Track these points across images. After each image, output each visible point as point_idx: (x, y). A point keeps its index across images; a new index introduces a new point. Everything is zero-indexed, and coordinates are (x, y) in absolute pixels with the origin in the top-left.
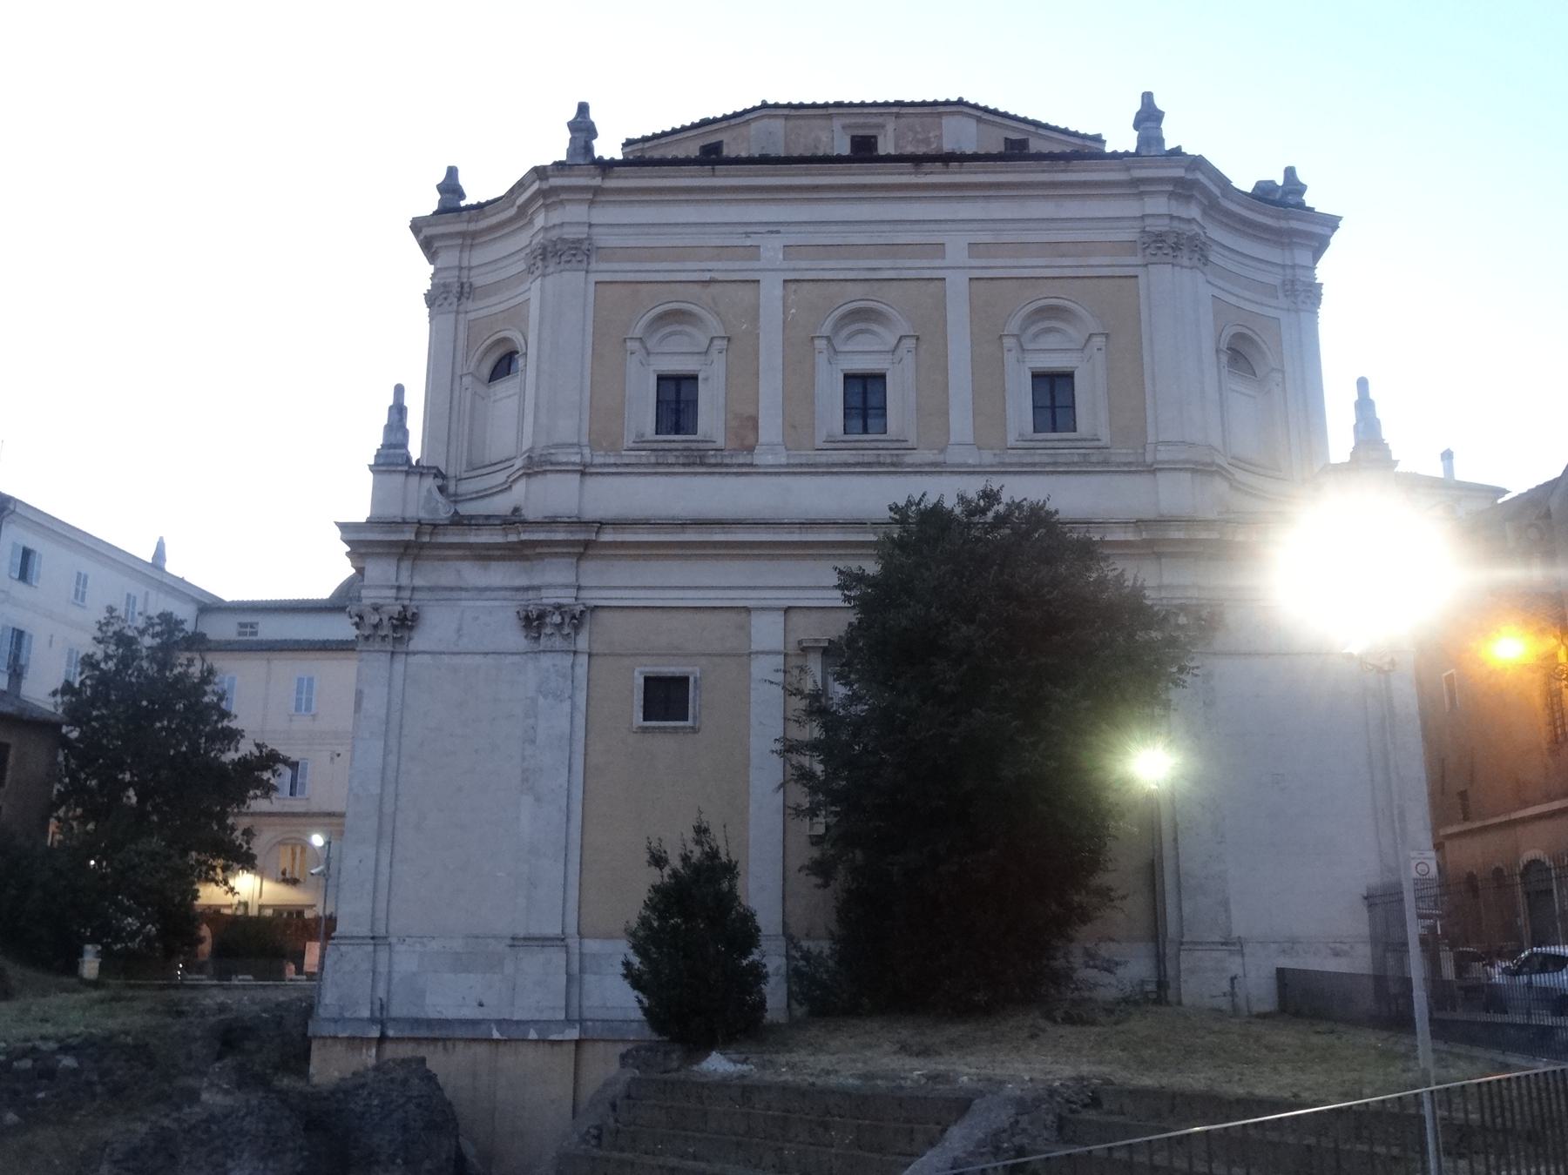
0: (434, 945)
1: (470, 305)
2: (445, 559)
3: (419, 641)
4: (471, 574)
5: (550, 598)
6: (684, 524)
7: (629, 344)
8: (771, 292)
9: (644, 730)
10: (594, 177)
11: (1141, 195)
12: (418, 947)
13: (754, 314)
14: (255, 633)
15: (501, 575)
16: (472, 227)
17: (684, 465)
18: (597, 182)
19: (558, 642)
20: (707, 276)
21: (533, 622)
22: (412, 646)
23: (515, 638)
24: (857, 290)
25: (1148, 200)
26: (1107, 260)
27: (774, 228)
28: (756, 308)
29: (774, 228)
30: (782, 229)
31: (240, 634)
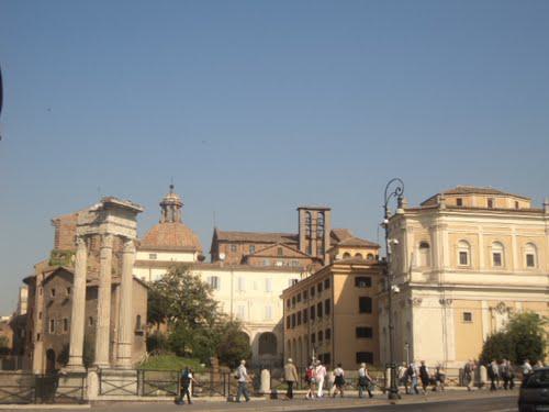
5: (446, 298)
15: (435, 292)
21: (442, 302)
23: (440, 305)
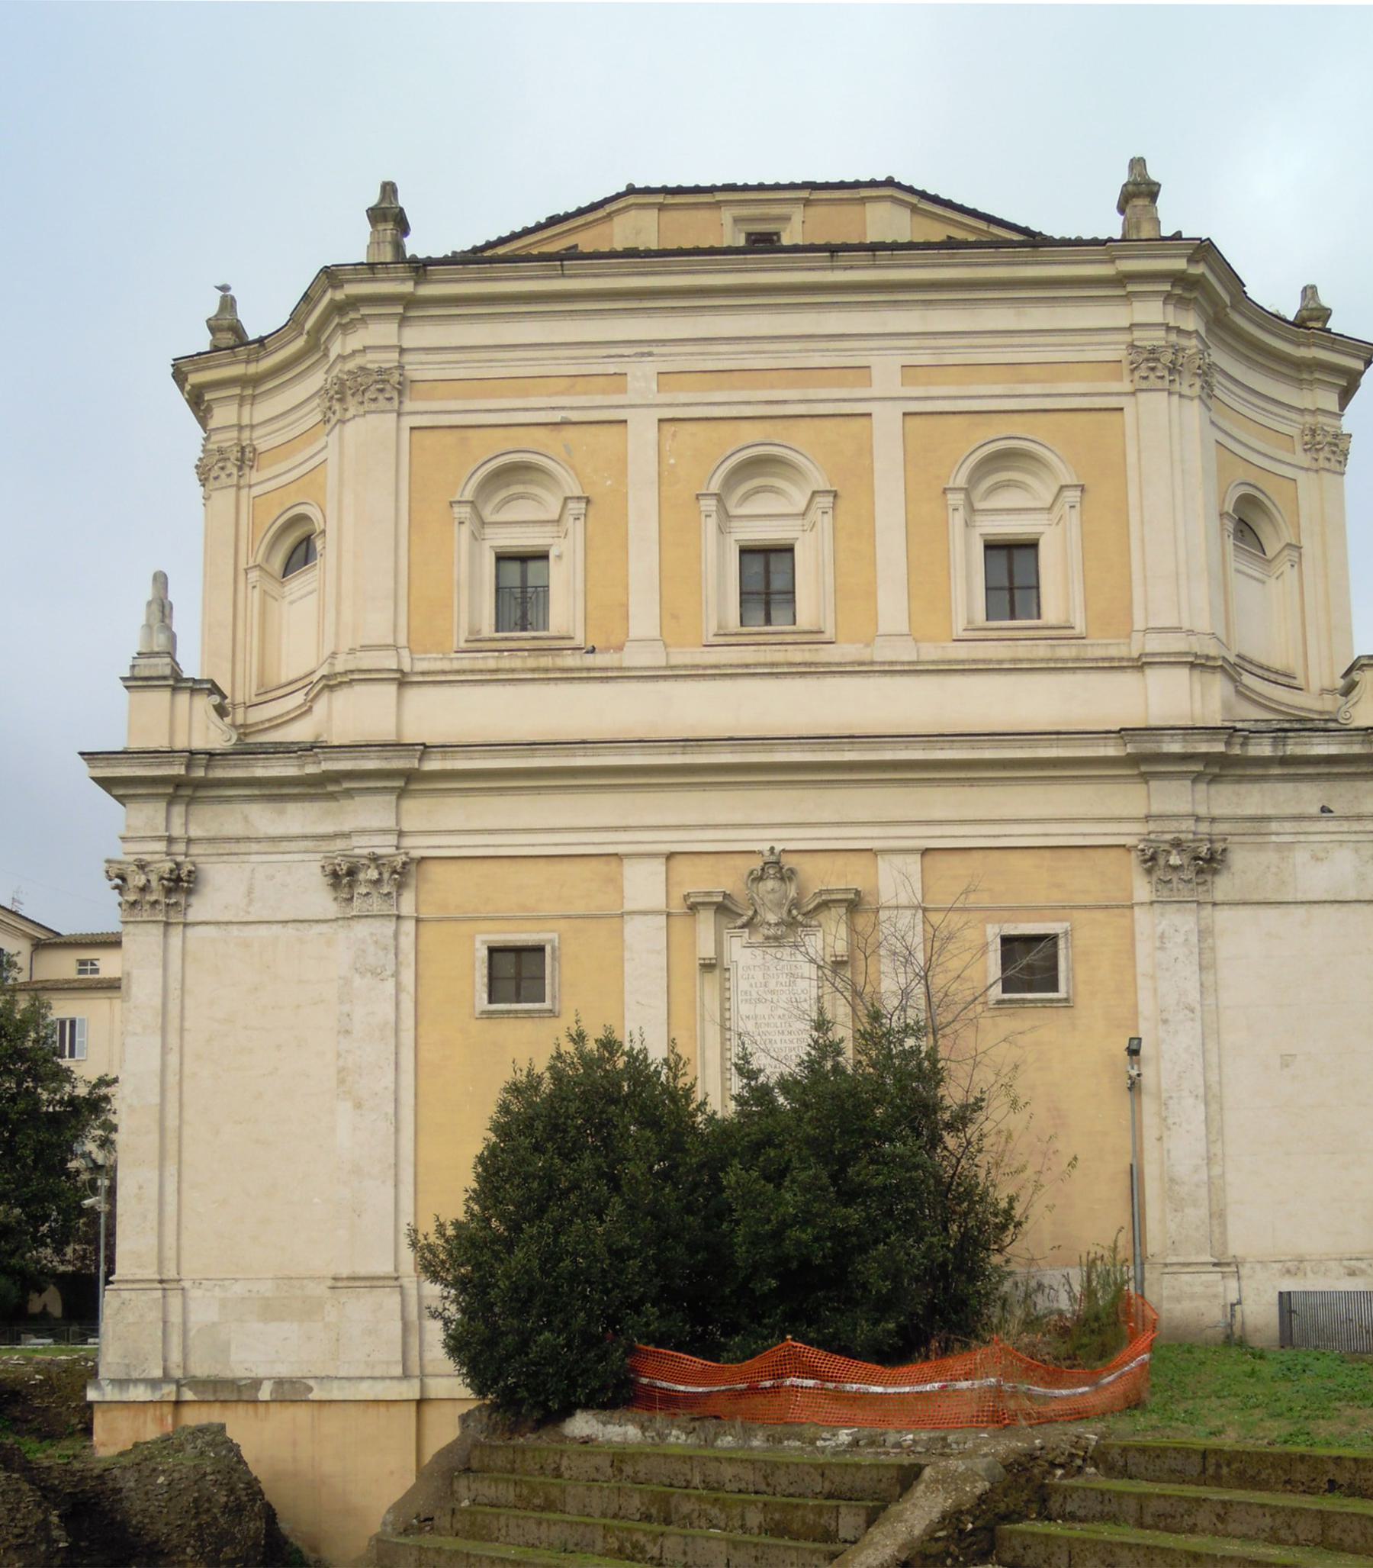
0: (238, 1289)
1: (254, 476)
2: (228, 800)
3: (200, 908)
4: (263, 819)
6: (533, 746)
7: (456, 509)
8: (887, 421)
9: (489, 1015)
10: (403, 280)
11: (1129, 297)
12: (217, 1292)
13: (620, 464)
14: (96, 971)
16: (253, 369)
17: (533, 670)
18: (407, 287)
19: (376, 905)
20: (557, 416)
22: (192, 917)
23: (322, 901)
24: (751, 433)
25: (1137, 305)
26: (998, 389)
27: (645, 347)
28: (623, 460)
29: (645, 347)
30: (655, 350)
31: (80, 972)
